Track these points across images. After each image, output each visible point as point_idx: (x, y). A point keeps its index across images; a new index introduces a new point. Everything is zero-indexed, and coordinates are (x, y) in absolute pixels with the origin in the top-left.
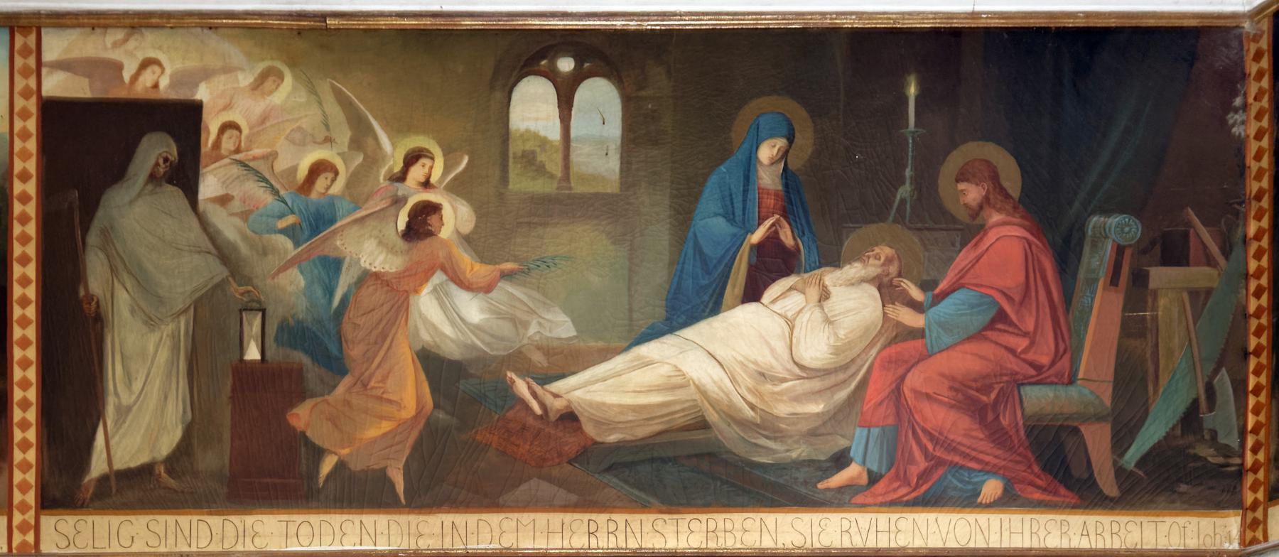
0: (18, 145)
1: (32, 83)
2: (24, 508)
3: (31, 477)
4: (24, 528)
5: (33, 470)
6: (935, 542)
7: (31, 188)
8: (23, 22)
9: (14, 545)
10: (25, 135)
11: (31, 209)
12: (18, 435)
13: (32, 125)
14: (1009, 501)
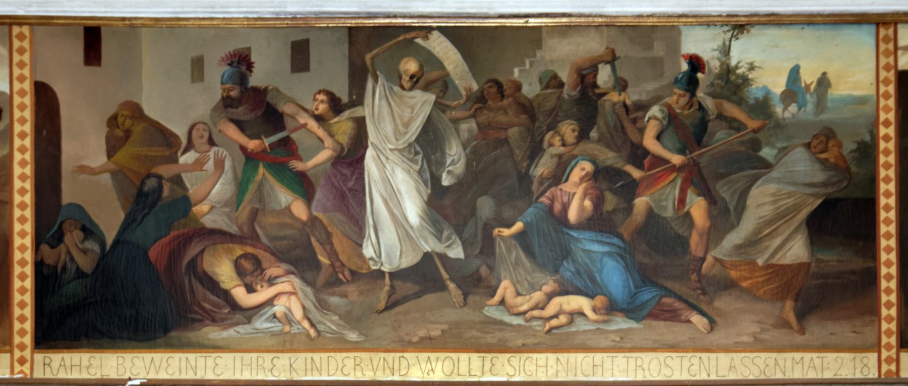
0: (882, 103)
1: (891, 60)
2: (889, 347)
3: (893, 326)
4: (889, 360)
5: (894, 323)
6: (227, 376)
7: (891, 131)
8: (889, 19)
9: (883, 371)
10: (887, 96)
11: (891, 145)
12: (884, 298)
13: (891, 89)
14: (759, 345)
